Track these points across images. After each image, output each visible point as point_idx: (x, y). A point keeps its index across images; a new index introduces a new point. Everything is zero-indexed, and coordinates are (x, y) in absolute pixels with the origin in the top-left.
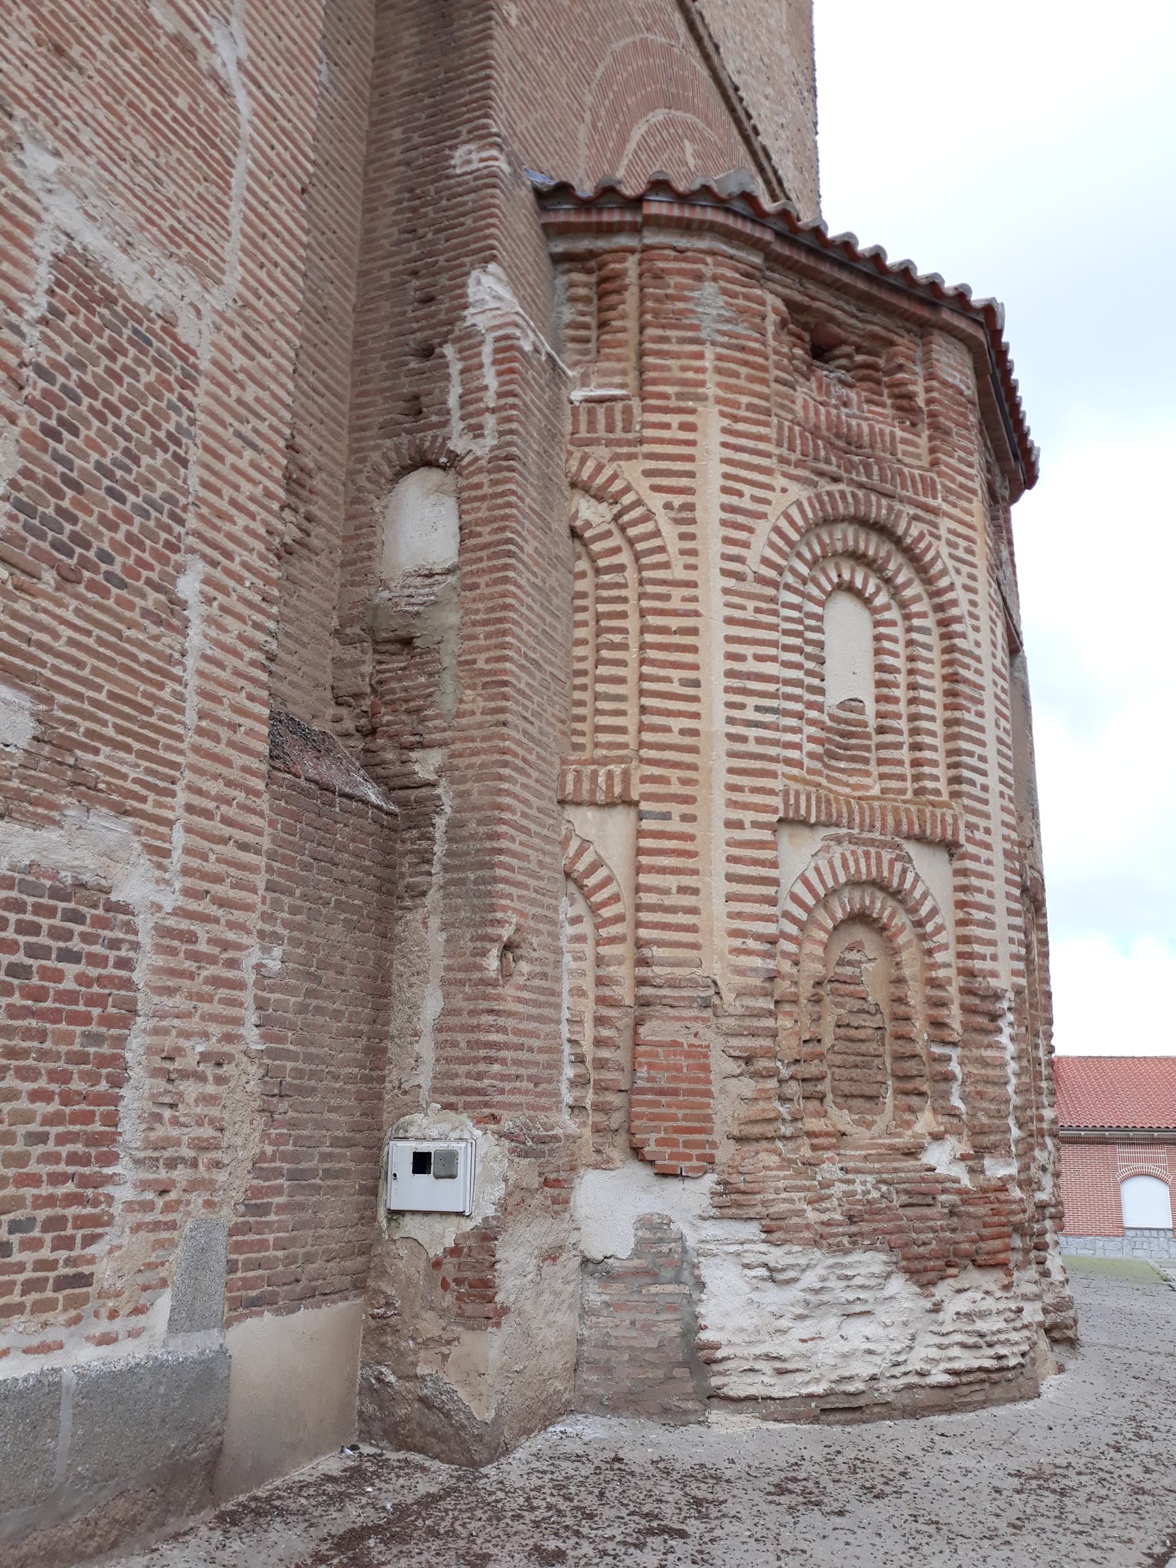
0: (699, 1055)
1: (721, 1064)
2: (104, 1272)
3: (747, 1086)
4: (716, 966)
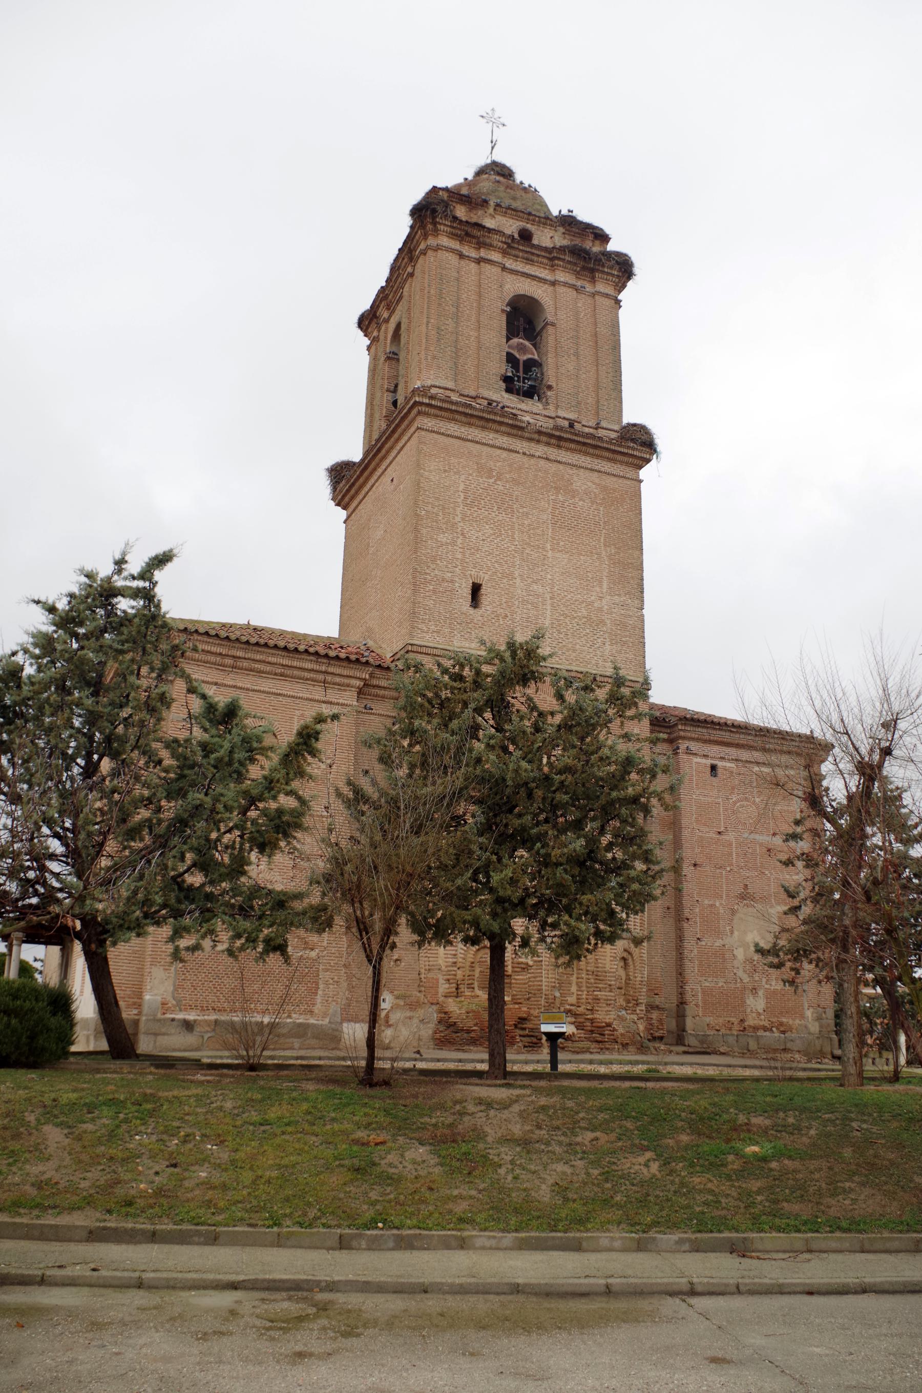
0: (437, 980)
1: (441, 981)
2: (316, 1011)
3: (447, 986)
4: (441, 962)
